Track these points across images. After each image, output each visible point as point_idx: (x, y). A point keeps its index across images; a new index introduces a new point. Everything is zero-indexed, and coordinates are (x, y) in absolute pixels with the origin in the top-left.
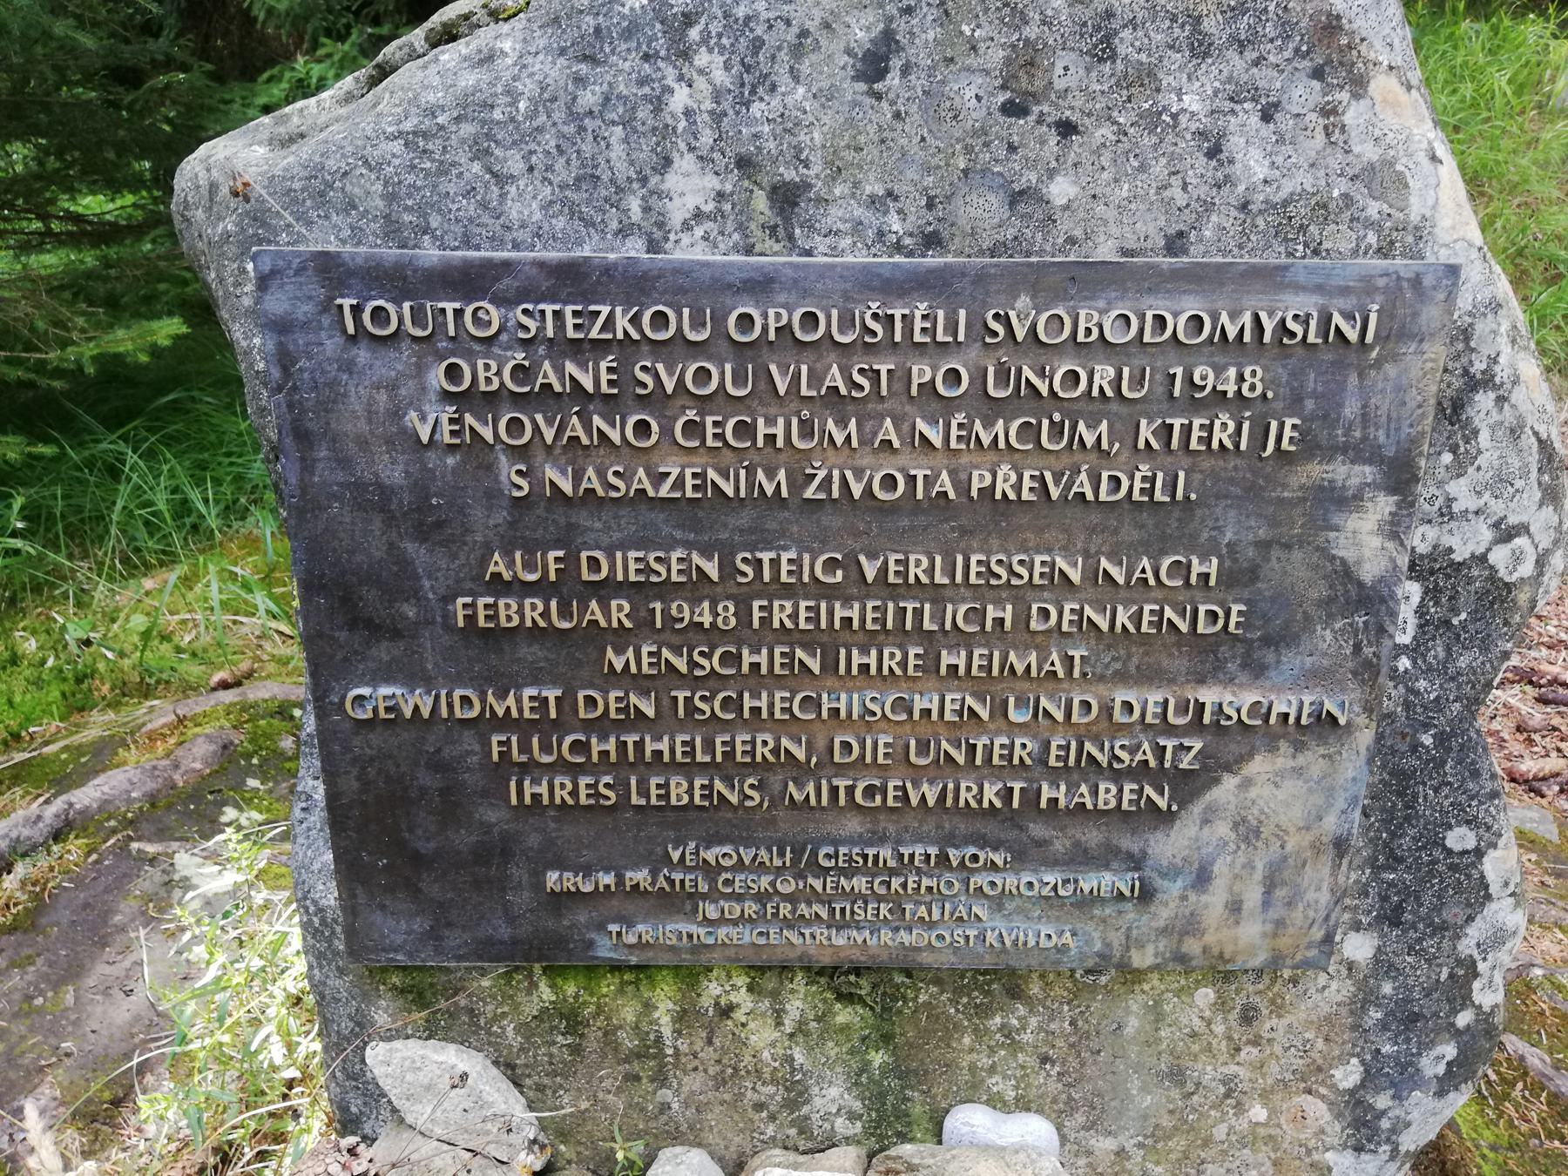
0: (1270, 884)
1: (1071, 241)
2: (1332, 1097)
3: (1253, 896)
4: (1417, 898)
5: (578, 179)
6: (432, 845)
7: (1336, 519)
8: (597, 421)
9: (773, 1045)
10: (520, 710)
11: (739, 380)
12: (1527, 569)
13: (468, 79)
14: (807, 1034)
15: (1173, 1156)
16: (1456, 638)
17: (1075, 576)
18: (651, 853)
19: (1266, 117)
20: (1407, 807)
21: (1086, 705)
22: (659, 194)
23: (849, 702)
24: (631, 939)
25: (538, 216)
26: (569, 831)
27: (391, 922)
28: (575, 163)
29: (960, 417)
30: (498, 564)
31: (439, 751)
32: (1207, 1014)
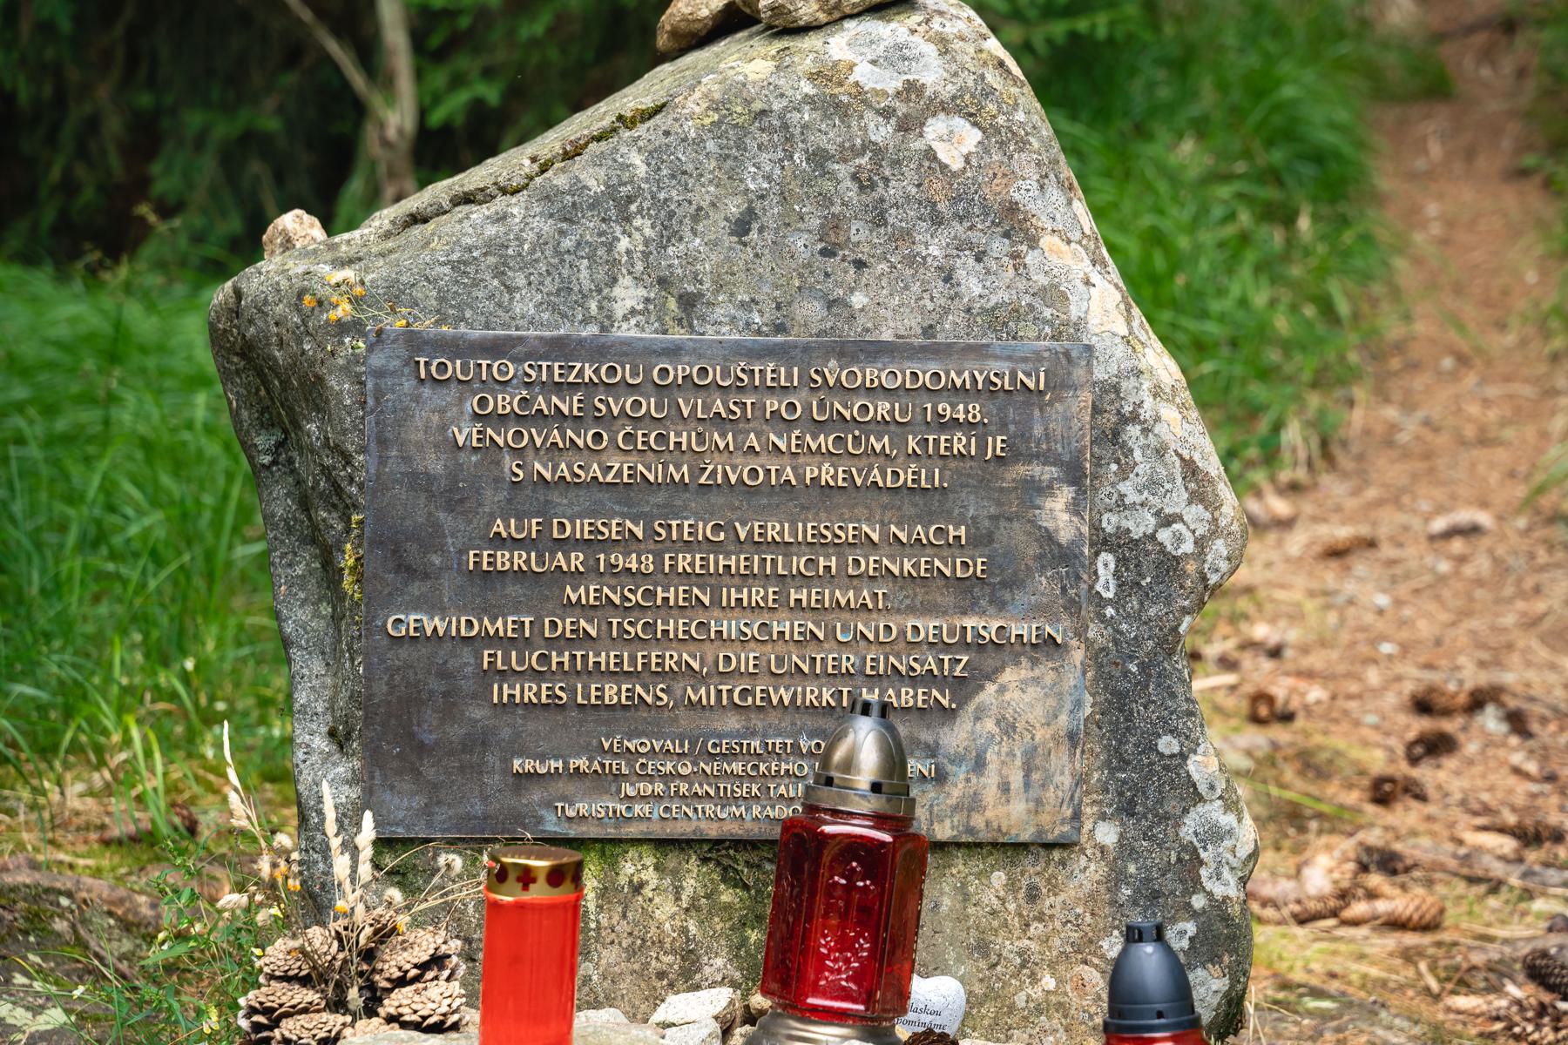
0: (1028, 770)
1: (867, 330)
2: (1103, 966)
3: (1016, 779)
4: (1144, 793)
5: (559, 290)
6: (434, 736)
7: (1038, 502)
8: (569, 433)
9: (673, 917)
10: (506, 631)
11: (659, 408)
12: (1188, 547)
13: (491, 230)
14: (698, 909)
15: (986, 1022)
16: (1146, 596)
17: (875, 537)
18: (589, 744)
19: (978, 260)
20: (1127, 720)
21: (888, 628)
22: (609, 299)
23: (730, 627)
24: (571, 813)
25: (532, 311)
26: (531, 726)
27: (397, 801)
28: (557, 280)
29: (797, 433)
30: (499, 526)
31: (445, 663)
32: (1002, 894)
